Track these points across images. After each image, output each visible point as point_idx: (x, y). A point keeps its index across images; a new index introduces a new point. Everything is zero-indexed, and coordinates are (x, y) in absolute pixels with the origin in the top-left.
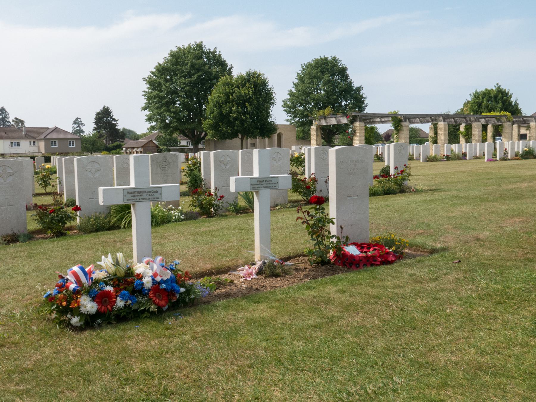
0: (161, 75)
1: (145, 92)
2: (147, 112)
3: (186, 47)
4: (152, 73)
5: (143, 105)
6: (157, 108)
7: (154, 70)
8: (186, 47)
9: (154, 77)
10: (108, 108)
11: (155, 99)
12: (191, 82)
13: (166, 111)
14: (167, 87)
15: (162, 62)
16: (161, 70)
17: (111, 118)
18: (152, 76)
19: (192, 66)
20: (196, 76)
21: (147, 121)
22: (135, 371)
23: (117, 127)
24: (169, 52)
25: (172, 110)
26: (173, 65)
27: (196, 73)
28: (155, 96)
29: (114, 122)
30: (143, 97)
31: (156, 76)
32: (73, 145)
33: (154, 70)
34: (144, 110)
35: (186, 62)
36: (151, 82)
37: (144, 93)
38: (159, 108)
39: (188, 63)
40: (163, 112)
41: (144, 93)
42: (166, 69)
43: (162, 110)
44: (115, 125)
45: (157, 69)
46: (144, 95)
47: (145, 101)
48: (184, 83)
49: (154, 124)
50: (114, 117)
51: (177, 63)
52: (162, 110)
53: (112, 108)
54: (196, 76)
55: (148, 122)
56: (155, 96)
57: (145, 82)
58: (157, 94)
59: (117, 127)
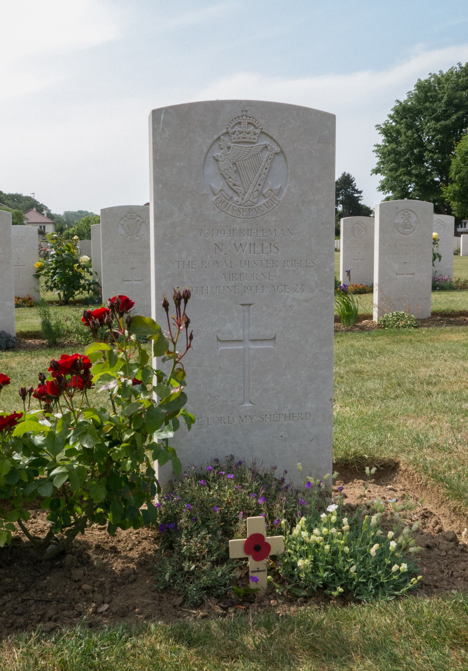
0: (401, 119)
1: (378, 146)
2: (381, 177)
3: (445, 73)
4: (390, 116)
5: (375, 166)
6: (391, 170)
7: (392, 113)
8: (445, 73)
9: (394, 124)
10: (349, 175)
11: (389, 155)
12: (445, 127)
13: (405, 174)
14: (407, 137)
15: (403, 98)
16: (404, 113)
17: (353, 189)
18: (391, 121)
19: (449, 103)
20: (454, 117)
21: (380, 190)
22: (425, 385)
23: (360, 202)
24: (415, 82)
25: (413, 171)
26: (419, 103)
27: (456, 112)
28: (389, 151)
29: (356, 195)
30: (375, 154)
31: (395, 121)
32: (465, 227)
33: (392, 113)
34: (376, 173)
35: (440, 96)
36: (386, 131)
37: (376, 148)
38: (395, 170)
39: (442, 98)
40: (400, 175)
41: (376, 148)
42: (409, 109)
43: (398, 173)
44: (357, 199)
45: (397, 111)
46: (377, 151)
47: (378, 160)
48: (435, 130)
49: (390, 194)
50: (356, 188)
51: (426, 99)
52: (398, 173)
53: (353, 175)
54: (454, 117)
55: (382, 192)
56: (389, 151)
57: (379, 131)
58: (392, 149)
59: (360, 202)
